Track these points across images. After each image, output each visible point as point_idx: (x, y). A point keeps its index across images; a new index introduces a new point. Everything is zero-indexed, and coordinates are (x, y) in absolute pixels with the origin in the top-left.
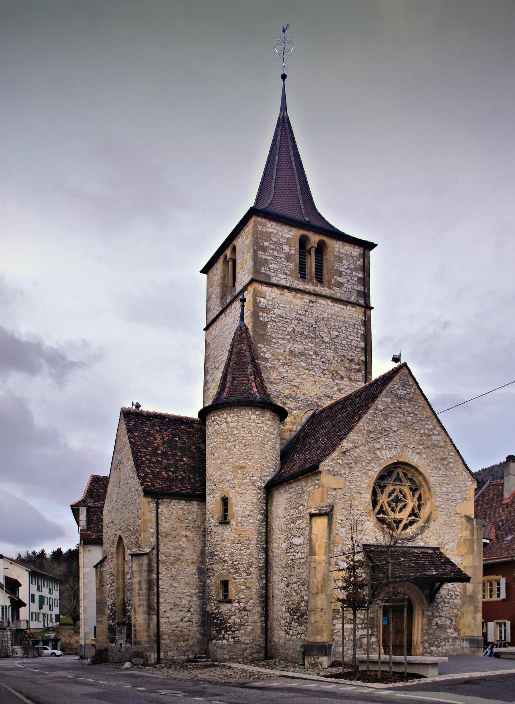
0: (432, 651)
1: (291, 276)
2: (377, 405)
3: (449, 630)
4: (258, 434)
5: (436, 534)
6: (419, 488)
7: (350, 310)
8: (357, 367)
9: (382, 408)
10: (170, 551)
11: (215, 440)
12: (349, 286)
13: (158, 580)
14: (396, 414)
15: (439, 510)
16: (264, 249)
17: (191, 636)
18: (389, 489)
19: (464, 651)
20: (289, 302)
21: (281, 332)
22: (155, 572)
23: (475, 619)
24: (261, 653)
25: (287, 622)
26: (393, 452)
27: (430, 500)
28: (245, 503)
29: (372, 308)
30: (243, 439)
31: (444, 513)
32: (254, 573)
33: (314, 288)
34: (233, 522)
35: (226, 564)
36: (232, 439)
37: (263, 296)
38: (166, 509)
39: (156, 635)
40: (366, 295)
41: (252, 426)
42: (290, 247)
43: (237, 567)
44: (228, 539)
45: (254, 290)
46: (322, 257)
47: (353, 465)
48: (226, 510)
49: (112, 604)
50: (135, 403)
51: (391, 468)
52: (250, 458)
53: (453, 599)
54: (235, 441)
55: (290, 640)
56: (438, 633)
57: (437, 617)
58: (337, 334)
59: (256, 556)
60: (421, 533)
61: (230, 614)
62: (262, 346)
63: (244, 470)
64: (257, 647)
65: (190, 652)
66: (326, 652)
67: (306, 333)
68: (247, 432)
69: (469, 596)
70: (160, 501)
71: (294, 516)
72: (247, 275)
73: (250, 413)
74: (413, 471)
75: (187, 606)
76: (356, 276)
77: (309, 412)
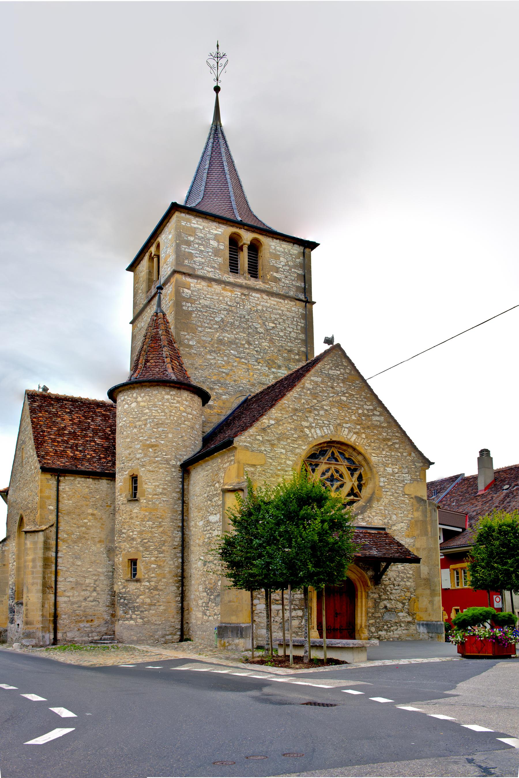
0: (380, 635)
1: (220, 269)
2: (304, 384)
3: (401, 614)
4: (173, 414)
5: (380, 514)
6: (359, 468)
7: (288, 303)
8: (297, 357)
9: (311, 387)
10: (72, 529)
11: (124, 419)
12: (288, 282)
13: (57, 557)
14: (328, 394)
15: (383, 490)
16: (188, 243)
17: (96, 617)
18: (323, 467)
19: (421, 636)
20: (217, 294)
21: (208, 321)
22: (54, 549)
23: (431, 602)
24: (175, 634)
25: (204, 602)
26: (325, 430)
27: (373, 480)
28: (158, 482)
29: (314, 303)
30: (155, 418)
31: (389, 493)
32: (167, 552)
33: (246, 282)
34: (143, 501)
35: (135, 542)
36: (143, 418)
37: (186, 287)
38: (69, 487)
39: (53, 615)
40: (307, 290)
41: (166, 406)
42: (218, 242)
43: (147, 545)
44: (137, 517)
45: (177, 281)
46: (257, 255)
47: (276, 442)
48: (136, 488)
49: (13, 583)
50: (42, 386)
51: (324, 447)
52: (163, 437)
53: (405, 582)
54: (146, 420)
55: (208, 622)
56: (387, 617)
57: (385, 599)
58: (273, 325)
59: (170, 535)
60: (362, 513)
61: (138, 593)
62: (186, 333)
63: (156, 448)
64: (171, 629)
65: (94, 634)
66: (241, 634)
67: (237, 323)
68: (159, 411)
69: (424, 579)
70: (61, 478)
71: (211, 493)
72: (170, 268)
73: (163, 393)
74: (350, 450)
75: (92, 585)
76: (295, 272)
77: (240, 398)
